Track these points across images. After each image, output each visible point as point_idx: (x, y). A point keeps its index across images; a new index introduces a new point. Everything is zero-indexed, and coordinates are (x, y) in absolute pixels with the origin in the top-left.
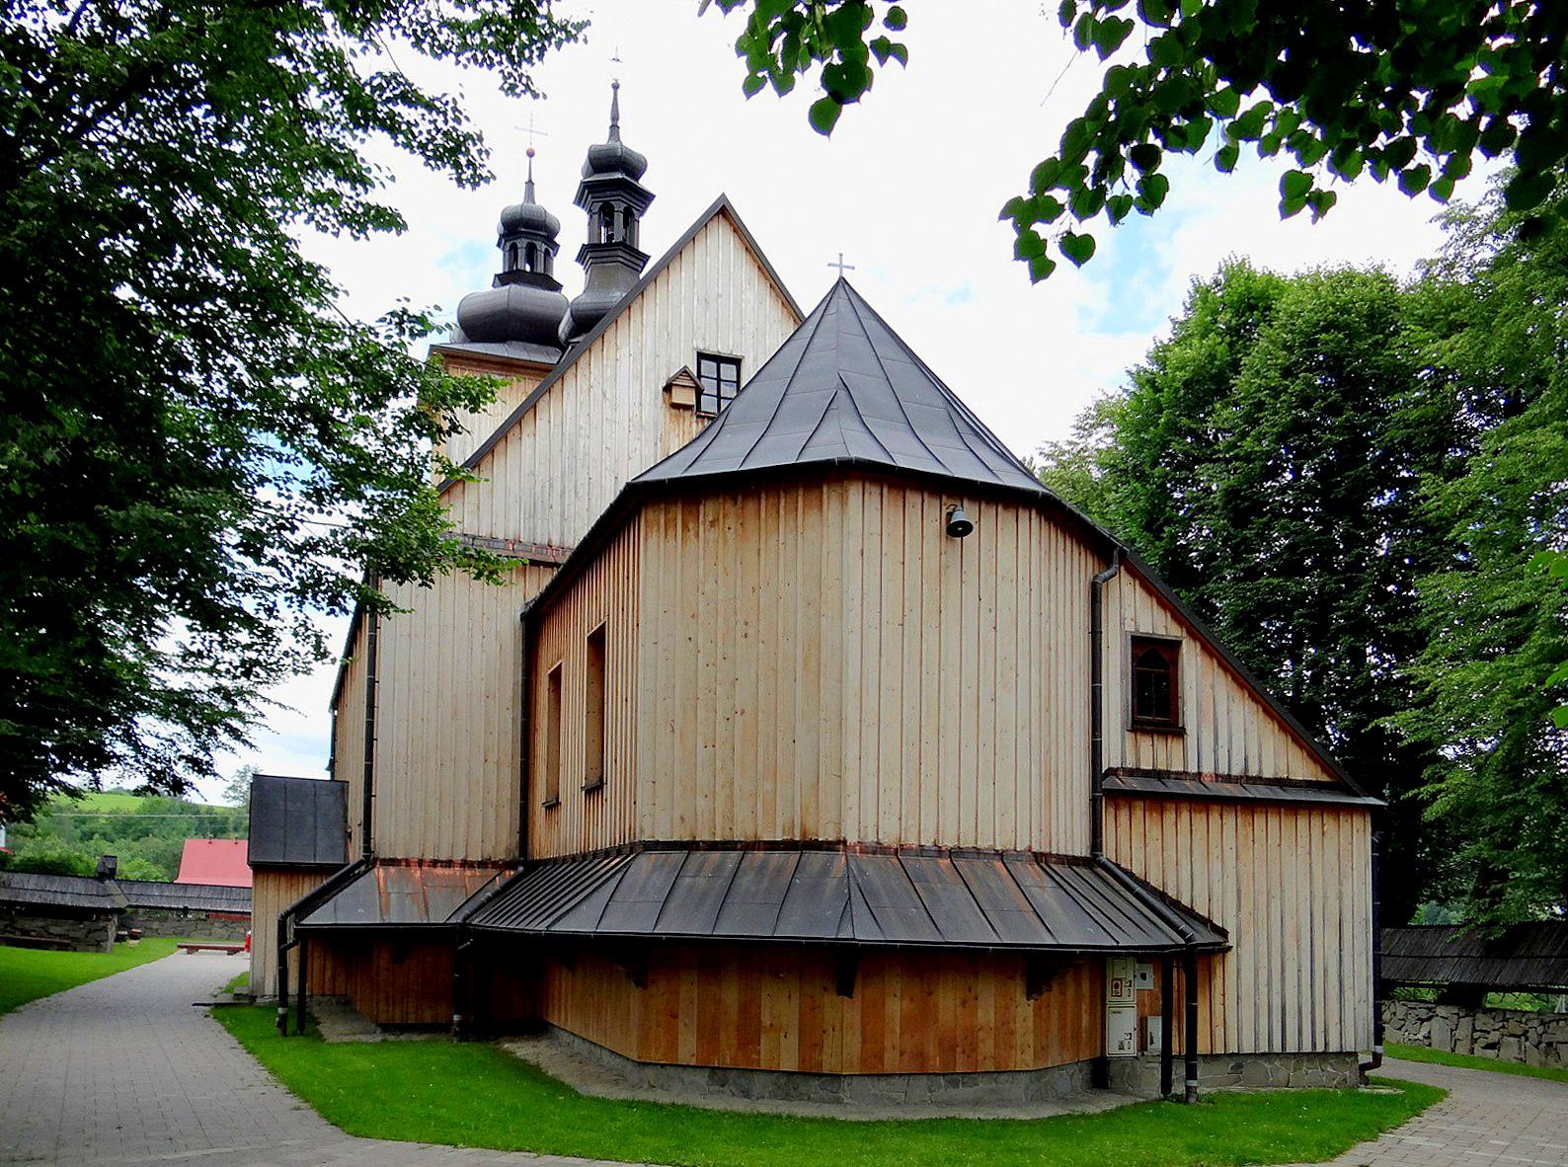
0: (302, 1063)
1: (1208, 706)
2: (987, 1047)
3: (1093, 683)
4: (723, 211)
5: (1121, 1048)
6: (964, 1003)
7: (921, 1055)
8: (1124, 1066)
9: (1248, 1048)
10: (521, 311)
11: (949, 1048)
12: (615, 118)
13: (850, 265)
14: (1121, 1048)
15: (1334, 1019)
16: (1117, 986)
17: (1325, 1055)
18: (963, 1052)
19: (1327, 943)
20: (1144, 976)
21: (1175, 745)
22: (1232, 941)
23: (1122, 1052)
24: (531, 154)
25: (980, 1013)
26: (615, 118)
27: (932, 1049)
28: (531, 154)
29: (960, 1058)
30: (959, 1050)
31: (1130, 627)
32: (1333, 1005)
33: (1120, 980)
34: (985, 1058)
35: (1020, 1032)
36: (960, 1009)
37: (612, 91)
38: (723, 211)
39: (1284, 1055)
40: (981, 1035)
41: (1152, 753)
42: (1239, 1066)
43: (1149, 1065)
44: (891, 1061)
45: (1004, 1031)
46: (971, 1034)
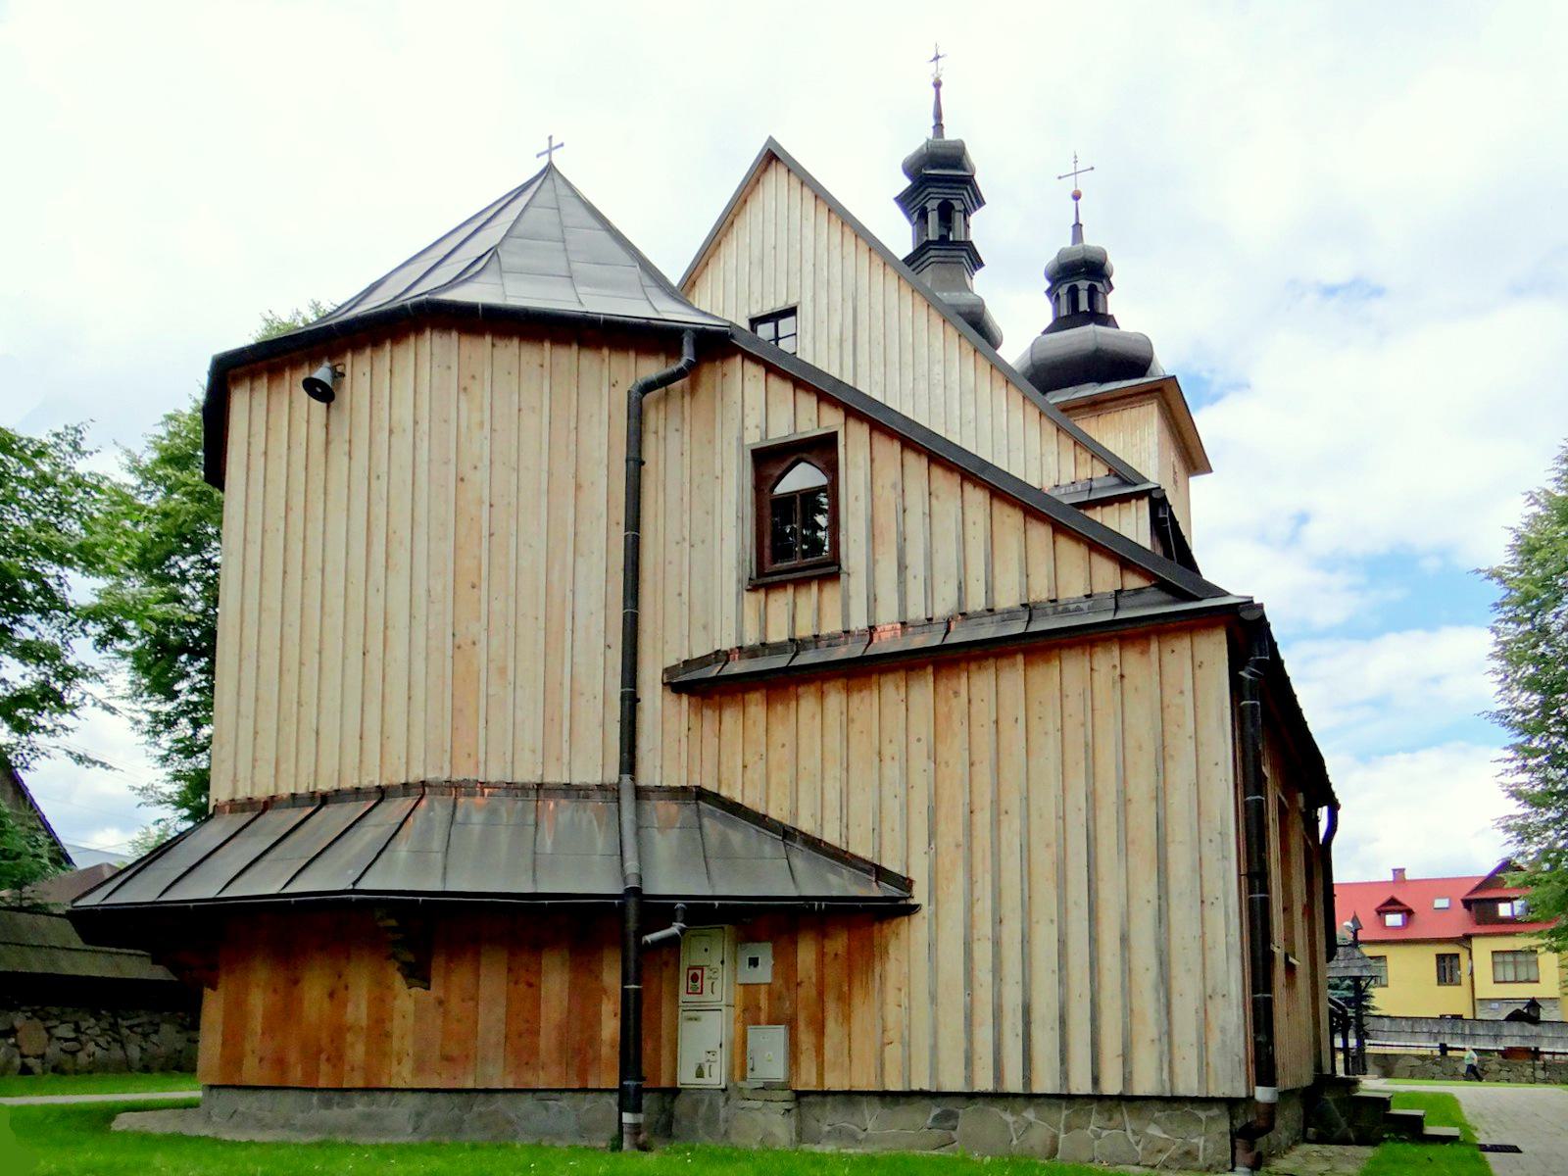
0: (1153, 1130)
1: (887, 519)
2: (357, 1051)
3: (638, 538)
4: (772, 157)
5: (700, 1074)
6: (331, 995)
7: (280, 1063)
8: (696, 1104)
9: (953, 1082)
10: (1046, 359)
11: (312, 1055)
12: (938, 116)
13: (547, 141)
14: (700, 1074)
15: (1147, 1028)
16: (695, 978)
17: (1127, 1100)
18: (328, 1060)
19: (1124, 888)
20: (754, 962)
21: (831, 594)
22: (919, 895)
23: (700, 1081)
24: (1077, 197)
25: (350, 1008)
26: (938, 116)
27: (293, 1057)
28: (1077, 197)
29: (324, 1067)
30: (323, 1057)
31: (754, 439)
32: (1146, 1001)
33: (701, 968)
34: (353, 1069)
35: (397, 1033)
36: (327, 1000)
37: (933, 90)
38: (772, 157)
39: (998, 1097)
40: (349, 1038)
41: (794, 616)
42: (947, 1118)
43: (747, 1104)
44: (252, 1071)
45: (379, 1031)
46: (339, 1031)
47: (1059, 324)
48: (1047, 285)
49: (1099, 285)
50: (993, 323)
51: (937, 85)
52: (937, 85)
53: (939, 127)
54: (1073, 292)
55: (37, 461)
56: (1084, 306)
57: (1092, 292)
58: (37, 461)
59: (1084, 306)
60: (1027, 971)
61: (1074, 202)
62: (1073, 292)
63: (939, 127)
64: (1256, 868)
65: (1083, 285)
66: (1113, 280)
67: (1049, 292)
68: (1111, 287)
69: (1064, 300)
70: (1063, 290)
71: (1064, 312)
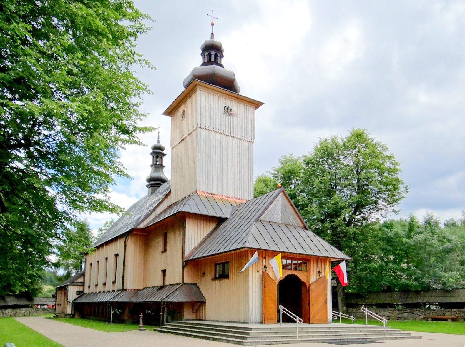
12: (159, 139)
24: (213, 25)
26: (159, 139)
28: (213, 25)
47: (204, 64)
48: (201, 52)
49: (219, 55)
50: (91, 327)
51: (159, 132)
52: (159, 132)
53: (158, 141)
54: (210, 55)
55: (104, 66)
56: (213, 59)
57: (216, 56)
58: (104, 66)
59: (213, 59)
60: (299, 342)
61: (211, 26)
62: (210, 55)
63: (158, 141)
64: (335, 300)
65: (213, 53)
66: (224, 54)
67: (201, 54)
68: (223, 56)
69: (206, 57)
70: (206, 54)
71: (206, 61)
